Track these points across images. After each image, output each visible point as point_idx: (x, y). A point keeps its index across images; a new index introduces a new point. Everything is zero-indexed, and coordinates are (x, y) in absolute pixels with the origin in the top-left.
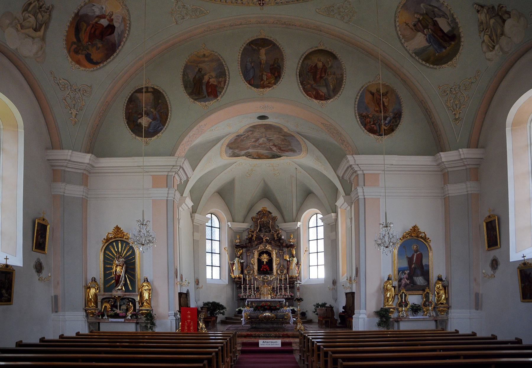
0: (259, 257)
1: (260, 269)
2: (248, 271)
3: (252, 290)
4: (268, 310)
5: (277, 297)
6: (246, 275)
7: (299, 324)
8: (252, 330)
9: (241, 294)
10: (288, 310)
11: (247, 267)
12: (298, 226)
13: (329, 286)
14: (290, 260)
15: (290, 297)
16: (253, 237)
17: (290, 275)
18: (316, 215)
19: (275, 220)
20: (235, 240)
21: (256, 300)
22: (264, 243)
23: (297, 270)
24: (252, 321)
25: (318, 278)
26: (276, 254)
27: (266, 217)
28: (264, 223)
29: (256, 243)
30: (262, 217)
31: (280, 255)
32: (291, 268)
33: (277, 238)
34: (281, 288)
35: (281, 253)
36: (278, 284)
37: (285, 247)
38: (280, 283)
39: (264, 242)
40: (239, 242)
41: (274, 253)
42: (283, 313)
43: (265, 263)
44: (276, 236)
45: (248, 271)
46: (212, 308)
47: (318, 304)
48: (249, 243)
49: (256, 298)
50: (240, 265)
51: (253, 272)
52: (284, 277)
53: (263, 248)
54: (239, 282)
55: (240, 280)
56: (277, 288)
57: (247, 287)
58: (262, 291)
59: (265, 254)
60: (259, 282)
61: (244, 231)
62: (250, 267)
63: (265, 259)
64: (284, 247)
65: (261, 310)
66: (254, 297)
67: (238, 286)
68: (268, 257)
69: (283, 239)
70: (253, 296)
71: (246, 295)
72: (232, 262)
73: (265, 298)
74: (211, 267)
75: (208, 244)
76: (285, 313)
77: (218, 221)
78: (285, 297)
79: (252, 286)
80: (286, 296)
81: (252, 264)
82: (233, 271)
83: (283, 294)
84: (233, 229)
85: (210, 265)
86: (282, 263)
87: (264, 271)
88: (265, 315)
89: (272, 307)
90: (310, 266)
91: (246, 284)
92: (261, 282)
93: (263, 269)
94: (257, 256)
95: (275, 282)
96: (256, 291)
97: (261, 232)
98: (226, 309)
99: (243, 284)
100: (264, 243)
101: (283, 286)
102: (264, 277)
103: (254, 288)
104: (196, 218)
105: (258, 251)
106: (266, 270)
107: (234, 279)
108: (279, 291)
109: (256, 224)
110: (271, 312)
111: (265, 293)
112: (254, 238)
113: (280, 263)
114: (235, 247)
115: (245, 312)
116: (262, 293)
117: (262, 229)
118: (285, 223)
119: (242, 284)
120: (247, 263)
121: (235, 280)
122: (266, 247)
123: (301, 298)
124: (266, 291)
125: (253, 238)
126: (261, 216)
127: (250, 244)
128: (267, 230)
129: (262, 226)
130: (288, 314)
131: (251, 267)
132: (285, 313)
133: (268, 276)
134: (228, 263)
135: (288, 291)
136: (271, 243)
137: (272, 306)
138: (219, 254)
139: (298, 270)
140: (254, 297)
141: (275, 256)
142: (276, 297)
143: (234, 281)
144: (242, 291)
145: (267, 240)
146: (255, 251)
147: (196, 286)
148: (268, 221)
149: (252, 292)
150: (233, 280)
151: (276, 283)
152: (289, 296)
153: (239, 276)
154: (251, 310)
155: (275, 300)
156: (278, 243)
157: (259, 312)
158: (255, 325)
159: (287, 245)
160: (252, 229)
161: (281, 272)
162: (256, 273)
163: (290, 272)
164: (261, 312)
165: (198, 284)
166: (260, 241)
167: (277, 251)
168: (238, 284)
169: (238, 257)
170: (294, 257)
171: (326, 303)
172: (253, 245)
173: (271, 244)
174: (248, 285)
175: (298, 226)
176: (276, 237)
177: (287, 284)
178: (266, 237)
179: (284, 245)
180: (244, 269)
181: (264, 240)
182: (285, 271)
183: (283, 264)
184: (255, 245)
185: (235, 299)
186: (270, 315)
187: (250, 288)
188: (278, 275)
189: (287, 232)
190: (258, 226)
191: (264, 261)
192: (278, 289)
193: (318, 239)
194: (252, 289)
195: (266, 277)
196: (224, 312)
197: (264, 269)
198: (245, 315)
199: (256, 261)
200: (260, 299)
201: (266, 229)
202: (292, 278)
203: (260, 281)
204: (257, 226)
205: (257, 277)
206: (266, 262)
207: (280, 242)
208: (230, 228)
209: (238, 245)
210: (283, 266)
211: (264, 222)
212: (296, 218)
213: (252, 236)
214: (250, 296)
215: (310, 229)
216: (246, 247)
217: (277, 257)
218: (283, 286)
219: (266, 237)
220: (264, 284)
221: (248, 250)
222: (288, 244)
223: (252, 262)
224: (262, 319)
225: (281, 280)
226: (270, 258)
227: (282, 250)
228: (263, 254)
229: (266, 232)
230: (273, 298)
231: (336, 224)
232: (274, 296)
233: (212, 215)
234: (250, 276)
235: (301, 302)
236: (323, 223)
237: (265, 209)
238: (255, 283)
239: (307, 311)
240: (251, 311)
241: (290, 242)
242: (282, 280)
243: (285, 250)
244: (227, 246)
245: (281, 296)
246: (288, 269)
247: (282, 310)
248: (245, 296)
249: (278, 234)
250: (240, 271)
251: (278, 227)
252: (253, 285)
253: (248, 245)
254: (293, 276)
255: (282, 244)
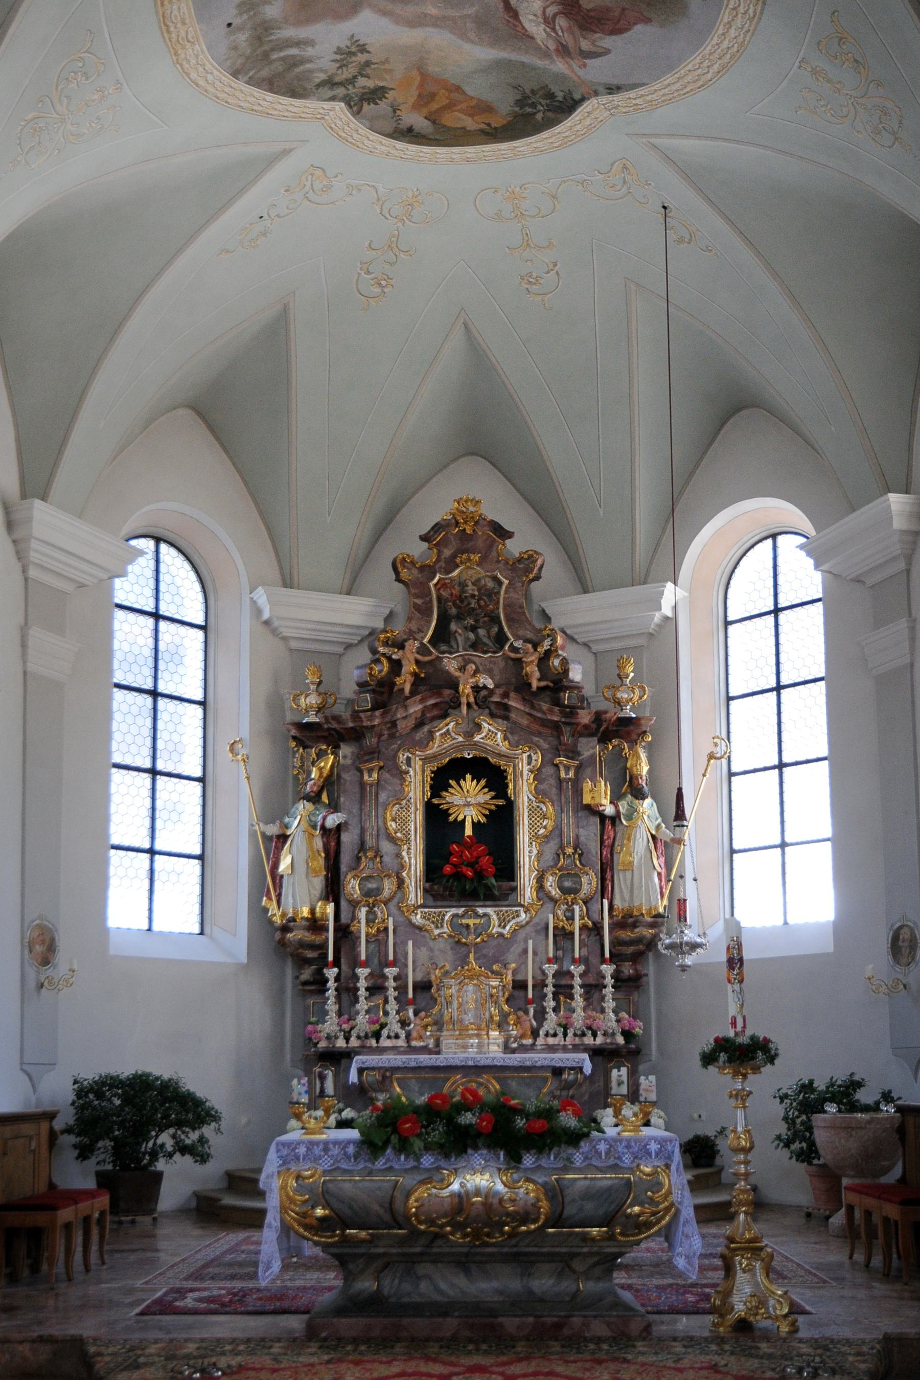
0: (433, 796)
1: (441, 868)
2: (368, 878)
3: (386, 1001)
4: (489, 1147)
5: (540, 1041)
6: (354, 904)
7: (749, 1270)
8: (348, 1325)
9: (324, 1022)
10: (653, 1147)
11: (359, 859)
12: (667, 610)
13: (869, 970)
14: (618, 812)
15: (620, 1040)
16: (399, 675)
17: (617, 902)
18: (770, 541)
19: (528, 570)
20: (296, 698)
21: (413, 1064)
22: (464, 709)
23: (659, 874)
24: (345, 1241)
25: (786, 923)
26: (538, 774)
27: (476, 557)
28: (463, 591)
29: (420, 707)
30: (454, 556)
31: (560, 781)
32: (620, 859)
33: (539, 680)
34: (563, 982)
35: (567, 768)
36: (549, 961)
37: (588, 731)
38: (560, 953)
39: (464, 700)
40: (319, 710)
41: (526, 768)
42: (615, 1168)
43: (468, 831)
44: (533, 671)
45: (368, 878)
46: (128, 1113)
47: (807, 1087)
48: (373, 709)
49: (411, 1050)
50: (319, 843)
51: (394, 888)
52: (582, 918)
53: (461, 739)
54: (312, 947)
55: (318, 939)
56: (540, 985)
57: (356, 978)
58: (449, 1004)
59: (468, 777)
60: (431, 950)
61: (349, 646)
62: (378, 853)
63: (468, 804)
64: (581, 735)
65: (427, 1148)
66: (401, 1043)
67: (306, 975)
68: (485, 797)
69: (577, 687)
70: (397, 1037)
71: (354, 1033)
72: (273, 830)
73: (465, 1047)
74: (146, 856)
75: (124, 728)
76: (631, 1170)
77: (197, 587)
78: (588, 1040)
79: (391, 972)
80: (595, 1035)
81: (392, 840)
82: (277, 880)
83: (579, 1018)
84: (287, 633)
85: (137, 844)
86: (570, 833)
87: (465, 876)
88: (455, 1187)
89: (520, 1122)
90: (733, 851)
91: (356, 963)
92: (443, 952)
93: (455, 866)
94: (419, 789)
95: (525, 951)
96: (412, 1002)
97: (444, 648)
98: (223, 1123)
99: (336, 963)
100: (464, 709)
101: (577, 970)
102: (463, 916)
103: (401, 989)
104: (37, 530)
105: (425, 760)
106: (475, 872)
107: (285, 929)
108: (552, 1004)
109: (419, 601)
110: (514, 1158)
111: (469, 1018)
112: (405, 682)
113: (558, 830)
114: (294, 738)
115: (285, 1161)
116: (446, 1018)
117: (453, 626)
118: (586, 591)
119: (331, 958)
120: (363, 831)
121: (290, 935)
122: (472, 736)
123: (761, 1035)
124: (472, 1006)
125: (398, 680)
126: (447, 553)
127: (378, 713)
128: (482, 632)
129: (454, 611)
130: (660, 1185)
131: (386, 859)
132: (631, 1170)
133: (489, 910)
134: (252, 834)
135: (610, 1004)
136: (506, 708)
137: (516, 1111)
138: (202, 780)
139: (663, 872)
140: (401, 1043)
141: (525, 788)
142: (534, 1044)
143: (282, 943)
144: (332, 1006)
145: (484, 693)
146: (408, 759)
147: (31, 973)
148: (491, 584)
149: (386, 1014)
150: (278, 935)
151: (535, 953)
152: (613, 1034)
153: (312, 911)
154: (336, 1143)
155: (528, 1064)
156: (545, 706)
157: (412, 1163)
158: (378, 1279)
159: (598, 717)
160: (398, 629)
161: (567, 884)
162: (414, 893)
163: (621, 881)
164: (427, 1160)
165: (46, 961)
166: (439, 694)
167: (538, 758)
168: (307, 962)
169: (308, 798)
170: (643, 797)
171: (856, 1078)
172: (401, 725)
173: (506, 718)
174: (364, 965)
175: (666, 609)
176: (537, 674)
177: (603, 961)
178: (477, 671)
179: (584, 717)
180: (343, 868)
181: (466, 689)
182: (589, 882)
183: (577, 837)
184: (411, 723)
185: (288, 1057)
186: (500, 1187)
187: (376, 989)
188: (550, 905)
189: (595, 654)
190: (432, 612)
191: (464, 820)
192: (549, 990)
193: (784, 681)
194: (392, 993)
195: (477, 916)
196: (202, 1140)
197: (464, 869)
198: (283, 1188)
199: (416, 820)
200: (438, 1053)
201: (473, 629)
202: (631, 920)
203: (441, 944)
204: (425, 611)
205: (418, 919)
206: (476, 825)
207: (557, 702)
208: (267, 623)
209: (309, 725)
210: (575, 849)
211: (463, 585)
212: (681, 493)
213: (396, 666)
214: (377, 1035)
215: (731, 628)
216: (356, 735)
217: (540, 794)
218: (577, 970)
219: (477, 671)
220: (464, 961)
221: (374, 753)
222: (606, 712)
223: (392, 825)
224: (431, 1222)
225: (563, 935)
226: (501, 802)
227: (573, 753)
228: (459, 777)
229: (475, 646)
230: (514, 1051)
231: (908, 571)
232: (523, 1036)
233: (163, 547)
234: (380, 912)
235: (756, 1070)
236: (818, 577)
237: (472, 509)
238: (407, 954)
239: (722, 1132)
240: (335, 1151)
241: (619, 703)
242: (572, 934)
243: (590, 748)
244: (245, 732)
245: (565, 1035)
246: (606, 870)
247: (602, 1147)
248: (347, 1039)
249: (548, 654)
250: (319, 883)
251: (547, 618)
252: (393, 964)
253: (371, 718)
254: (640, 909)
255: (570, 712)
